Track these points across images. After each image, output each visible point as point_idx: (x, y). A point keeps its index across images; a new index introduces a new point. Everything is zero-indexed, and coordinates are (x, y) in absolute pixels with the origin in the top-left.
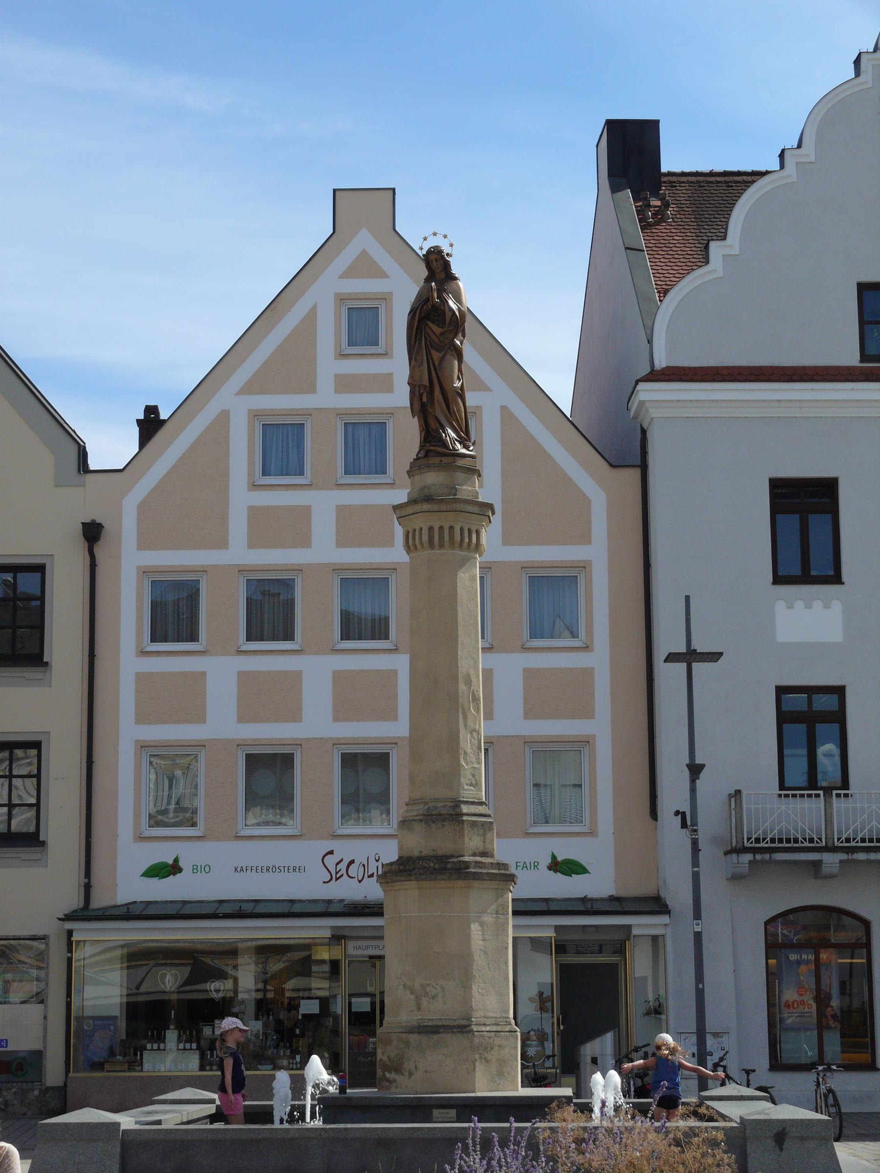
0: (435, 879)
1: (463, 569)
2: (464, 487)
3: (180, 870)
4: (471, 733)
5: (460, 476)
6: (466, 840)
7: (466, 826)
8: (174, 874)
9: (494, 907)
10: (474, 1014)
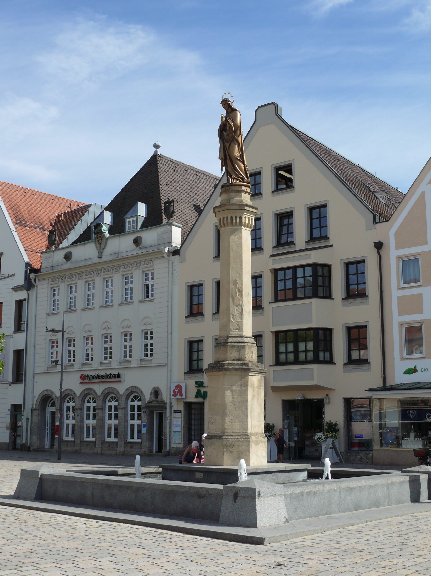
0: (212, 372)
1: (234, 234)
2: (235, 199)
3: (417, 371)
4: (237, 306)
5: (233, 194)
6: (229, 354)
7: (228, 347)
8: (415, 372)
9: (239, 383)
10: (227, 431)
